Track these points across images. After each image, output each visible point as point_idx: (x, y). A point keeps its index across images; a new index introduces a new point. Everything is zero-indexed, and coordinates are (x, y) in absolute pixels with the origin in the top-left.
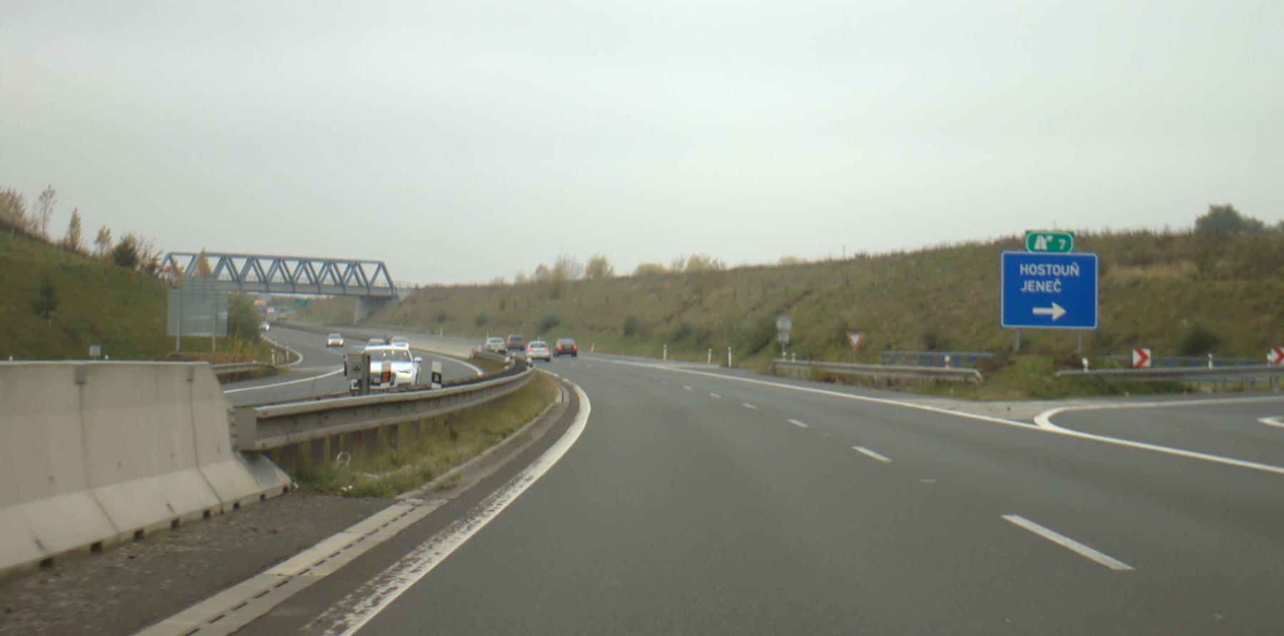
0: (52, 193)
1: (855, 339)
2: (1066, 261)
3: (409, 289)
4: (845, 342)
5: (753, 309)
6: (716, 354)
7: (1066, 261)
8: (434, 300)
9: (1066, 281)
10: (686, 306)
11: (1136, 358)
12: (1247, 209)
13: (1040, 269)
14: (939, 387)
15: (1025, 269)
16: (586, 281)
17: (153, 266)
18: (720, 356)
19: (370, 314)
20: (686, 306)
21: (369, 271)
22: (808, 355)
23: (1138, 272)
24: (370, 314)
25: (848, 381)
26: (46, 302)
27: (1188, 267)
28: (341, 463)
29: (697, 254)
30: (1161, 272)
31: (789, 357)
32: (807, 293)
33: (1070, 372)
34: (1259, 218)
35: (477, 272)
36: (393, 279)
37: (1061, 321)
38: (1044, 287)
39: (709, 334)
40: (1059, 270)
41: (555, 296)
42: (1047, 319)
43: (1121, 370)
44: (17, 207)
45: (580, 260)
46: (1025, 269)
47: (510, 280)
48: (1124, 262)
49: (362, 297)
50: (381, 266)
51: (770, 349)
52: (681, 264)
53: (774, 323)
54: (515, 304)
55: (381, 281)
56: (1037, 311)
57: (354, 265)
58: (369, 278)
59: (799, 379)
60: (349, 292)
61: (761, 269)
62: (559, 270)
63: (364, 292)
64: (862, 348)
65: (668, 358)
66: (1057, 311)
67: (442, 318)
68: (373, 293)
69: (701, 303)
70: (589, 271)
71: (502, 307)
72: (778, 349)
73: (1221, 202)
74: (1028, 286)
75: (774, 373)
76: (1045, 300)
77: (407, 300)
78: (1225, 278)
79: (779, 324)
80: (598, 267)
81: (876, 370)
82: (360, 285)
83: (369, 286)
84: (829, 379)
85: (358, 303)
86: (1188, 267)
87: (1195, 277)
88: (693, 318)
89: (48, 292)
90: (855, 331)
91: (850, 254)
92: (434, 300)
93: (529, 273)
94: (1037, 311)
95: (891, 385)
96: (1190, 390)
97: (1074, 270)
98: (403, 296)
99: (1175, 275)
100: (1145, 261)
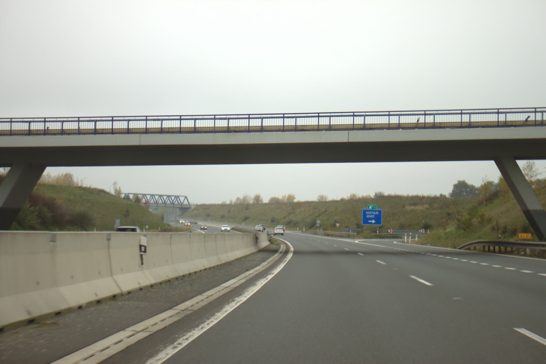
0: (117, 183)
1: (338, 225)
2: (375, 211)
3: (194, 205)
4: (334, 226)
5: (310, 216)
6: (300, 228)
7: (375, 211)
8: (204, 209)
9: (375, 215)
10: (290, 214)
11: (389, 231)
12: (470, 182)
13: (370, 213)
14: (349, 237)
15: (367, 213)
16: (253, 204)
17: (147, 203)
18: (301, 229)
19: (182, 214)
20: (290, 214)
21: (182, 199)
22: (325, 229)
23: (413, 207)
24: (182, 214)
25: (332, 235)
26: (127, 214)
27: (426, 206)
28: (240, 249)
29: (291, 194)
30: (419, 208)
31: (320, 230)
32: (325, 211)
33: (374, 234)
34: (474, 184)
35: (217, 200)
36: (190, 202)
37: (374, 223)
38: (371, 216)
39: (297, 223)
40: (374, 213)
41: (247, 209)
42: (371, 223)
43: (386, 233)
44: (71, 179)
45: (251, 195)
46: (367, 213)
47: (228, 202)
48: (410, 205)
49: (179, 208)
50: (186, 197)
51: (315, 227)
52: (285, 197)
53: (316, 220)
54: (233, 211)
55: (186, 202)
56: (369, 221)
57: (177, 197)
58: (182, 201)
59: (322, 235)
60: (176, 206)
61: (312, 202)
62: (245, 199)
63: (180, 206)
64: (340, 227)
65: (306, 230)
66: (373, 221)
67: (208, 216)
68: (183, 206)
69: (294, 213)
70: (254, 200)
71: (229, 212)
72: (317, 227)
73: (461, 179)
74: (368, 216)
75: (316, 234)
76: (371, 219)
77: (195, 208)
78: (435, 209)
79: (317, 222)
80: (257, 198)
81: (343, 233)
82: (179, 204)
83: (182, 204)
84: (328, 235)
85: (178, 210)
86: (426, 206)
87: (428, 209)
88: (292, 218)
89: (127, 211)
90: (338, 223)
91: (339, 199)
92: (204, 209)
93: (234, 200)
94: (369, 221)
95: (341, 236)
96: (401, 238)
97: (377, 213)
98: (193, 207)
99: (422, 208)
100: (415, 204)
